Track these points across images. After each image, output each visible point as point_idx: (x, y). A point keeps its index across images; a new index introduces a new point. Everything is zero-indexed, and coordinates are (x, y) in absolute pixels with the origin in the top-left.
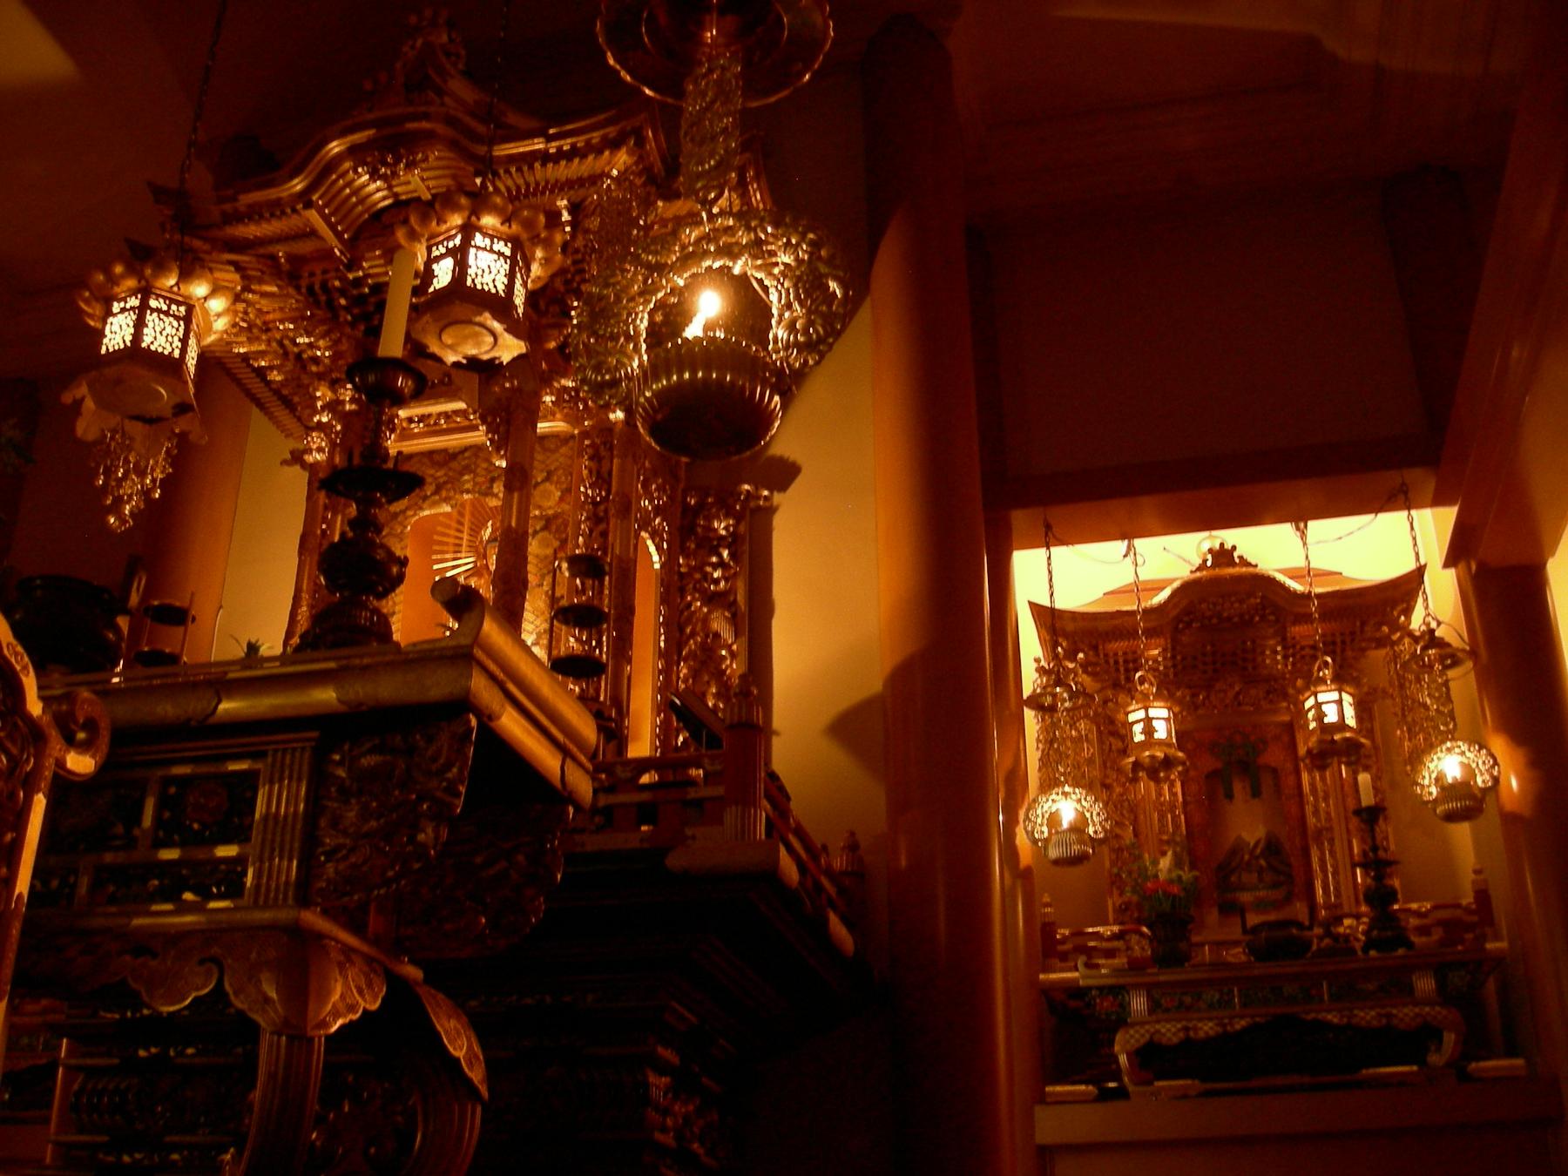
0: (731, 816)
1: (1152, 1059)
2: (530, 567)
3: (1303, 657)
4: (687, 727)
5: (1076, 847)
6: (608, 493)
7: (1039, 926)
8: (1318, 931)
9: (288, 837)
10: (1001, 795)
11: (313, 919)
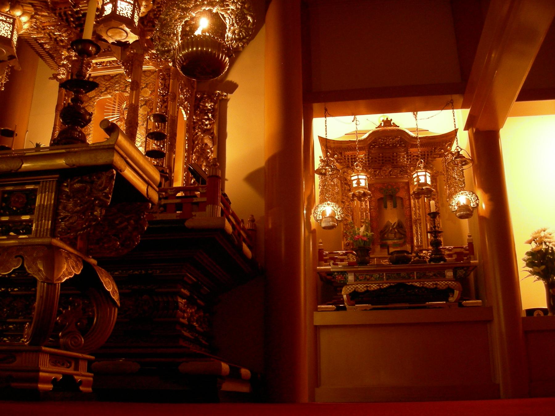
0: (209, 208)
1: (355, 297)
2: (139, 118)
3: (414, 159)
4: (195, 177)
5: (331, 223)
6: (168, 92)
7: (317, 250)
8: (414, 254)
9: (48, 212)
10: (306, 204)
11: (56, 242)
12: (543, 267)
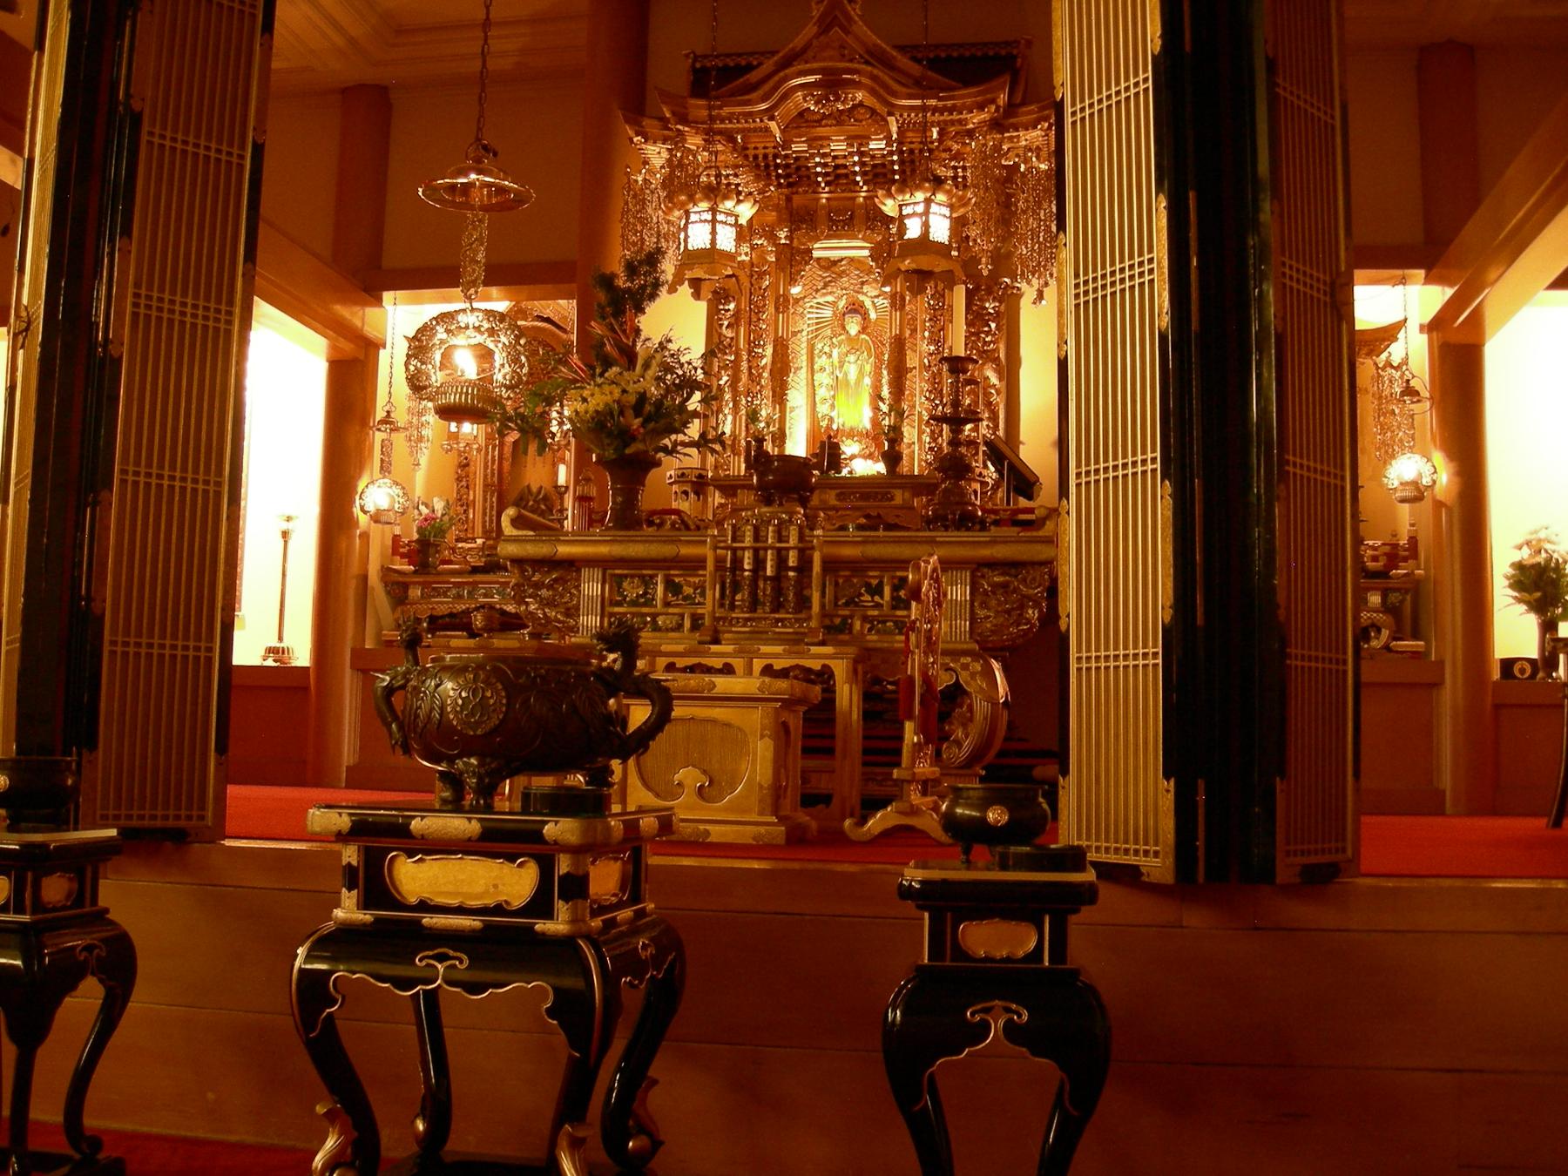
12: (1538, 594)
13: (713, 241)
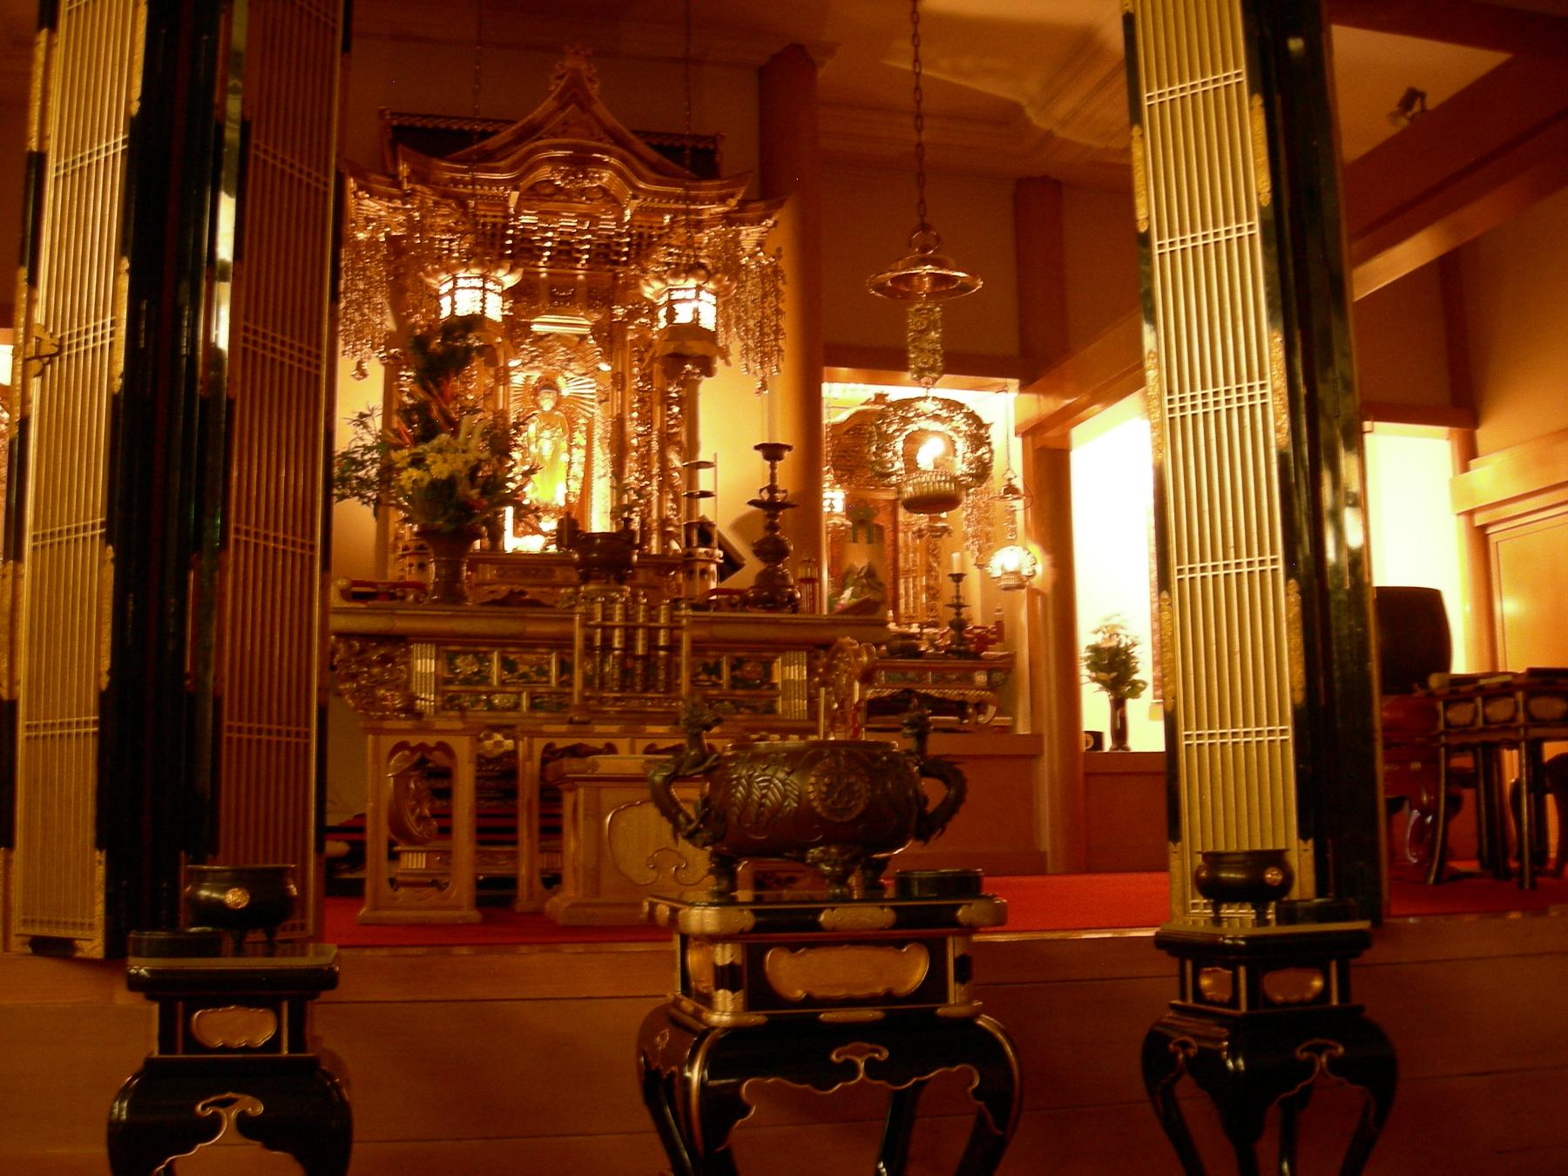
13: (483, 311)
